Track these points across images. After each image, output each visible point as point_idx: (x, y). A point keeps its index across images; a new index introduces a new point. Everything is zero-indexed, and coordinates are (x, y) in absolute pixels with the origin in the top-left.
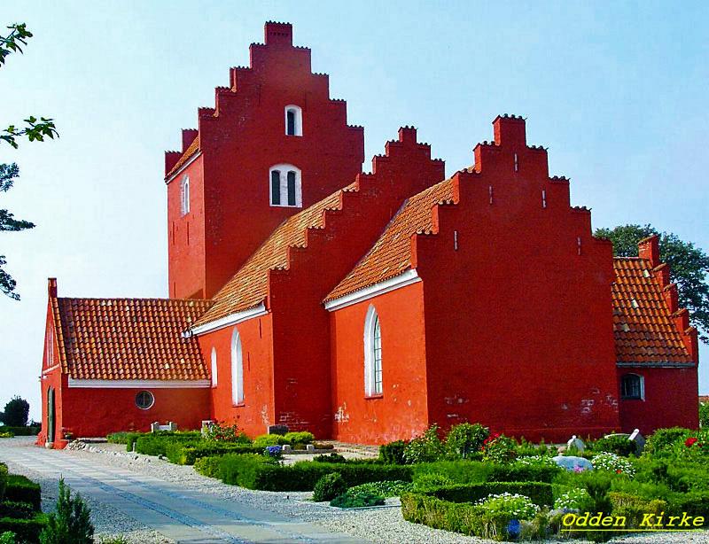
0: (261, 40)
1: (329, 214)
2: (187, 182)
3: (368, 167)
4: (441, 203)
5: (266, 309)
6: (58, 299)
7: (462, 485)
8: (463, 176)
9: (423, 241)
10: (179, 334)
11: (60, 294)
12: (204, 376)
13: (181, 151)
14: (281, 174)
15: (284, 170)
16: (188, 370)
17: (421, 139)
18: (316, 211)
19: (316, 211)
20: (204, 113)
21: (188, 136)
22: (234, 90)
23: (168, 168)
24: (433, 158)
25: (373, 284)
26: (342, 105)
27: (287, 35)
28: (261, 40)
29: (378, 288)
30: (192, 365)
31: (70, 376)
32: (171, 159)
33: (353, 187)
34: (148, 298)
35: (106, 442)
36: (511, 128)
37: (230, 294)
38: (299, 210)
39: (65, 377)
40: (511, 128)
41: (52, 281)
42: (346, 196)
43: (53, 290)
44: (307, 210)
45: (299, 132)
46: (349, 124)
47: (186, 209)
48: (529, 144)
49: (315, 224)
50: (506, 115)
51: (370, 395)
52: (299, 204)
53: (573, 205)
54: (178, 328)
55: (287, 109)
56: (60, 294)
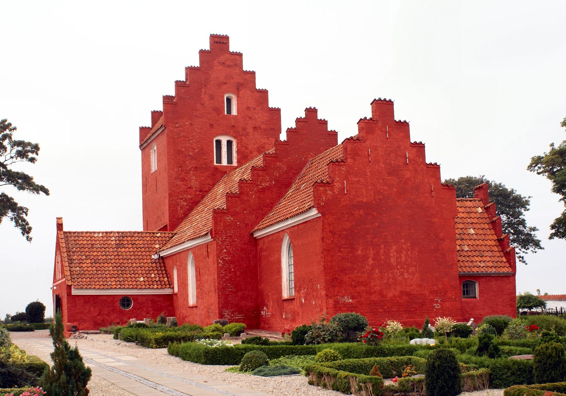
1: (254, 169)
11: (65, 229)
13: (150, 126)
19: (246, 169)
38: (235, 168)
43: (60, 226)
47: (154, 167)
48: (397, 118)
52: (235, 164)
56: (65, 229)
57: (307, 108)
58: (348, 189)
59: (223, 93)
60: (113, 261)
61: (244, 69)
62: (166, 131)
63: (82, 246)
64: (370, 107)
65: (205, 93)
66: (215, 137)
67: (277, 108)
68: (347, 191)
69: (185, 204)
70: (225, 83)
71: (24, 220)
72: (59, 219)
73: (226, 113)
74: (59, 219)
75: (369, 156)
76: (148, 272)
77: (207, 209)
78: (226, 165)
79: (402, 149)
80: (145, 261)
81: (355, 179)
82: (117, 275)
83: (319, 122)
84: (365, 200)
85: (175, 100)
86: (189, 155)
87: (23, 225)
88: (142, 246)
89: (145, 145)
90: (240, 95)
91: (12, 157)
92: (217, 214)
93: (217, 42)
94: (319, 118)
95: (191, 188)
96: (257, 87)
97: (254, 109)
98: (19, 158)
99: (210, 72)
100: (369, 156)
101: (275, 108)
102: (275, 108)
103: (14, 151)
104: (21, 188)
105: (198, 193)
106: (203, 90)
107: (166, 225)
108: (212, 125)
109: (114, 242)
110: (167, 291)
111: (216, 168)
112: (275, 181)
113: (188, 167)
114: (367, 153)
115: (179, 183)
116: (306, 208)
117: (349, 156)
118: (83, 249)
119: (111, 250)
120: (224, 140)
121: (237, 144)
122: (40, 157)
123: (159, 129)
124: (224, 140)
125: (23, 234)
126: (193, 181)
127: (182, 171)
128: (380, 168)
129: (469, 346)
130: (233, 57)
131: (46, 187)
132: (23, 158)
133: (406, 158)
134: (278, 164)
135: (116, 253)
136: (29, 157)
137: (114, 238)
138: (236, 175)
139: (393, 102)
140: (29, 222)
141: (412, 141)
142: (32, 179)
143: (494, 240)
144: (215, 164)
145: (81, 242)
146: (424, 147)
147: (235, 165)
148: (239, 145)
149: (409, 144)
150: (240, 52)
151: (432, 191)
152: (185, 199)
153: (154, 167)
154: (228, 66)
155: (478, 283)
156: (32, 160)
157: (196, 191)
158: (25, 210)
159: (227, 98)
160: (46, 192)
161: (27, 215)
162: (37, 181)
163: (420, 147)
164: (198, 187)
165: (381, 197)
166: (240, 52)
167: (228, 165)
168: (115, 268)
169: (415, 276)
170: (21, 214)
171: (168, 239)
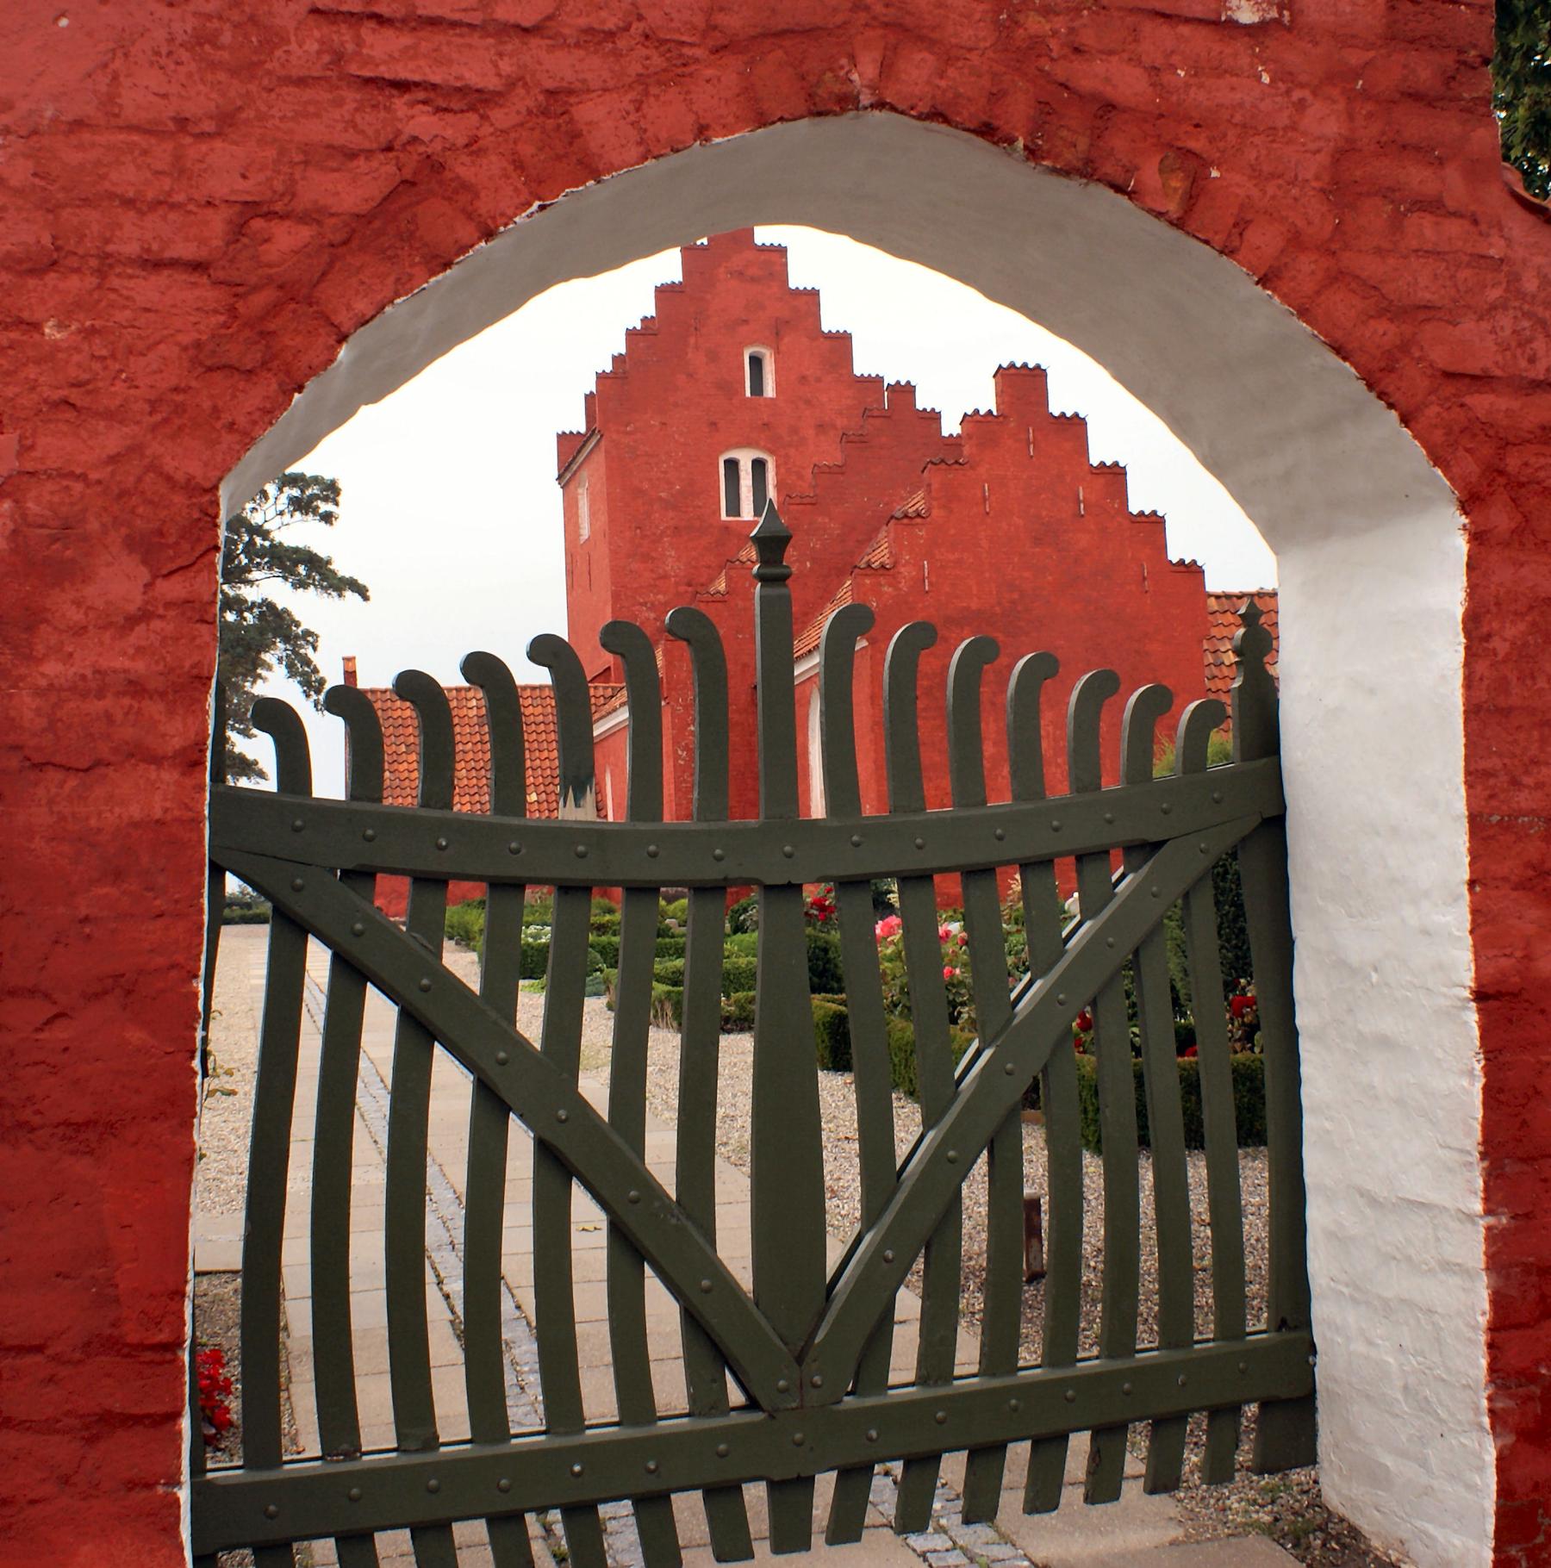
7: (219, 568)
14: (742, 464)
32: (569, 444)
46: (858, 371)
47: (585, 532)
48: (1055, 408)
50: (898, 382)
57: (1000, 366)
58: (934, 580)
59: (741, 346)
60: (471, 755)
61: (792, 285)
62: (603, 443)
63: (400, 721)
64: (992, 382)
65: (697, 348)
66: (722, 452)
68: (930, 584)
69: (652, 615)
70: (746, 322)
71: (307, 662)
72: (349, 660)
73: (748, 394)
74: (349, 660)
75: (985, 499)
76: (550, 779)
79: (1068, 479)
80: (546, 754)
81: (951, 557)
82: (476, 789)
83: (921, 415)
84: (974, 605)
86: (660, 499)
87: (303, 674)
88: (541, 718)
89: (568, 475)
90: (783, 348)
91: (281, 513)
94: (919, 406)
95: (665, 577)
96: (825, 328)
97: (819, 380)
98: (297, 514)
99: (709, 297)
100: (985, 499)
103: (283, 499)
104: (301, 584)
105: (682, 589)
106: (692, 340)
108: (714, 424)
109: (474, 712)
111: (726, 527)
112: (814, 560)
113: (657, 527)
114: (979, 495)
115: (635, 566)
117: (935, 503)
118: (401, 730)
119: (467, 729)
120: (745, 458)
121: (777, 467)
122: (345, 508)
124: (745, 458)
125: (308, 696)
126: (670, 560)
127: (643, 537)
128: (1012, 529)
130: (763, 257)
131: (361, 581)
132: (307, 514)
133: (1078, 502)
134: (820, 520)
135: (478, 738)
136: (321, 511)
137: (474, 702)
140: (319, 667)
141: (1094, 461)
142: (329, 562)
144: (724, 517)
145: (399, 713)
148: (783, 470)
149: (1087, 467)
151: (1144, 579)
152: (652, 604)
153: (585, 532)
154: (753, 280)
156: (327, 518)
157: (677, 584)
158: (310, 639)
159: (751, 358)
160: (362, 592)
161: (315, 649)
162: (342, 568)
163: (1115, 474)
164: (682, 574)
165: (1016, 596)
168: (474, 773)
170: (301, 647)
171: (602, 700)
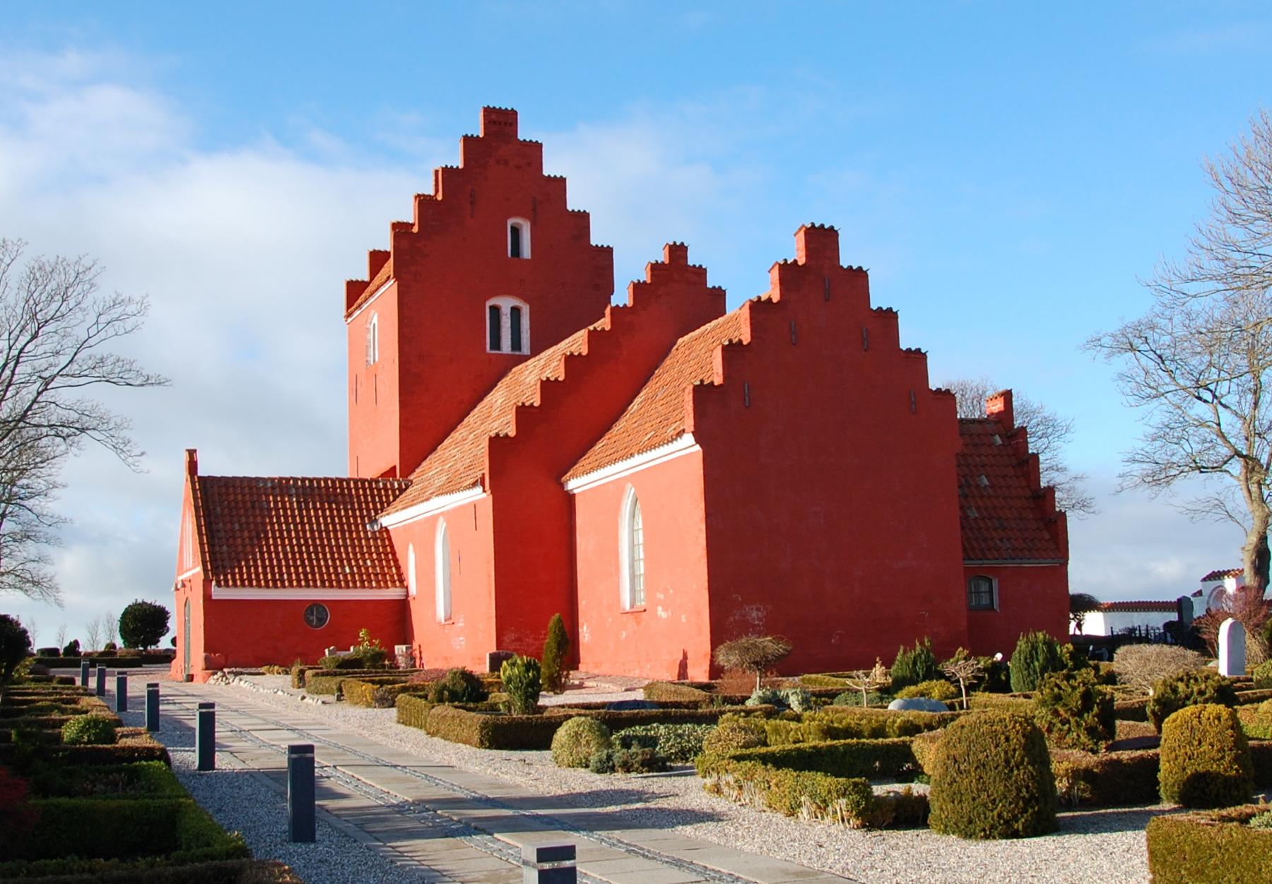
0: (479, 131)
1: (570, 360)
2: (375, 320)
3: (622, 296)
4: (727, 343)
5: (484, 491)
6: (199, 478)
8: (759, 308)
9: (703, 393)
10: (364, 526)
11: (202, 472)
12: (397, 583)
13: (367, 279)
15: (506, 304)
16: (376, 575)
17: (848, 258)
18: (550, 360)
19: (550, 360)
20: (400, 229)
21: (377, 259)
22: (440, 197)
23: (350, 303)
24: (709, 285)
25: (632, 455)
26: (583, 217)
27: (511, 124)
28: (479, 131)
29: (638, 459)
30: (382, 568)
31: (214, 583)
32: (355, 291)
33: (604, 323)
34: (322, 476)
35: (263, 674)
36: (677, 251)
37: (432, 469)
38: (526, 358)
39: (207, 583)
40: (677, 251)
41: (192, 453)
42: (593, 335)
43: (193, 466)
44: (537, 358)
45: (526, 252)
49: (549, 374)
51: (628, 608)
52: (526, 349)
53: (903, 346)
54: (362, 517)
55: (510, 222)
56: (202, 472)
67: (605, 246)
77: (472, 435)
78: (510, 353)
85: (415, 229)
92: (498, 444)
93: (494, 122)
101: (602, 246)
102: (602, 246)
107: (394, 468)
110: (393, 593)
116: (671, 434)
123: (382, 285)
129: (1076, 721)
138: (528, 372)
139: (836, 232)
143: (1026, 498)
146: (897, 317)
147: (525, 354)
150: (537, 142)
155: (997, 580)
159: (512, 228)
166: (537, 142)
167: (513, 353)
169: (1208, 610)
